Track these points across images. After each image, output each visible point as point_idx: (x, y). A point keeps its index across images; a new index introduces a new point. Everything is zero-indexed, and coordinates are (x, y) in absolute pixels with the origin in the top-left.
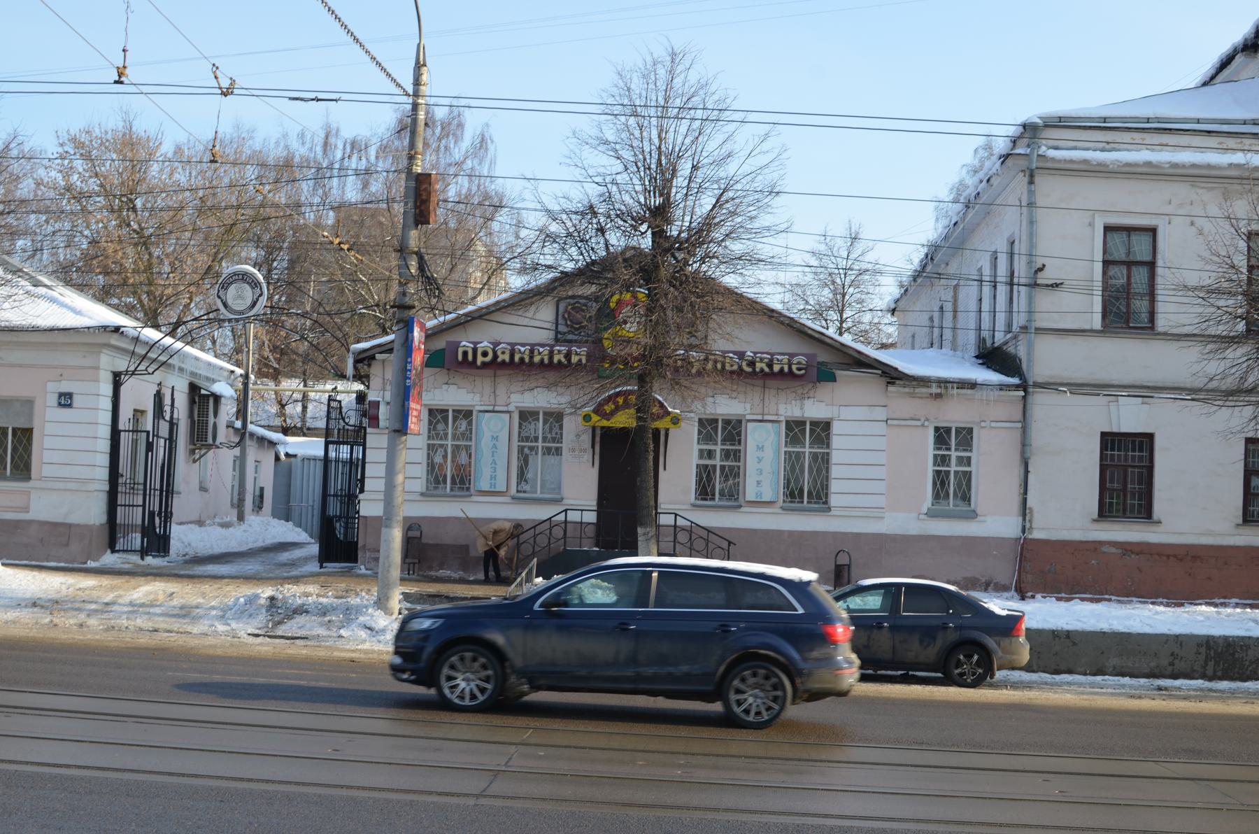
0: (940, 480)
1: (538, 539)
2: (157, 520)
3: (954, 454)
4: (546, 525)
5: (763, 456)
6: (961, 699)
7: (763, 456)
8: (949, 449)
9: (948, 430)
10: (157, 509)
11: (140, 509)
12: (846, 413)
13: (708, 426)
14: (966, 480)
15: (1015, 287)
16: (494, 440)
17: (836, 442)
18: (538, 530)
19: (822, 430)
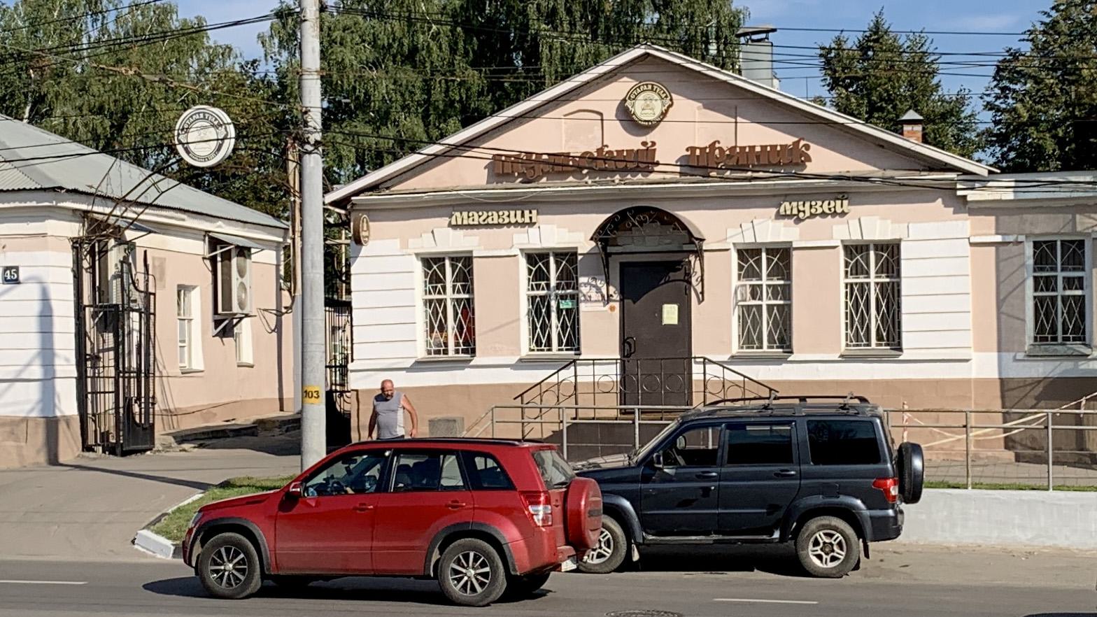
0: (1044, 309)
1: (545, 396)
2: (136, 409)
3: (1060, 275)
4: (536, 390)
5: (821, 292)
6: (1024, 174)
7: (821, 292)
8: (1054, 269)
9: (1052, 245)
10: (134, 394)
11: (112, 396)
12: (917, 230)
13: (748, 255)
14: (1078, 308)
15: (164, 379)
16: (505, 296)
17: (906, 268)
18: (527, 398)
19: (890, 253)
